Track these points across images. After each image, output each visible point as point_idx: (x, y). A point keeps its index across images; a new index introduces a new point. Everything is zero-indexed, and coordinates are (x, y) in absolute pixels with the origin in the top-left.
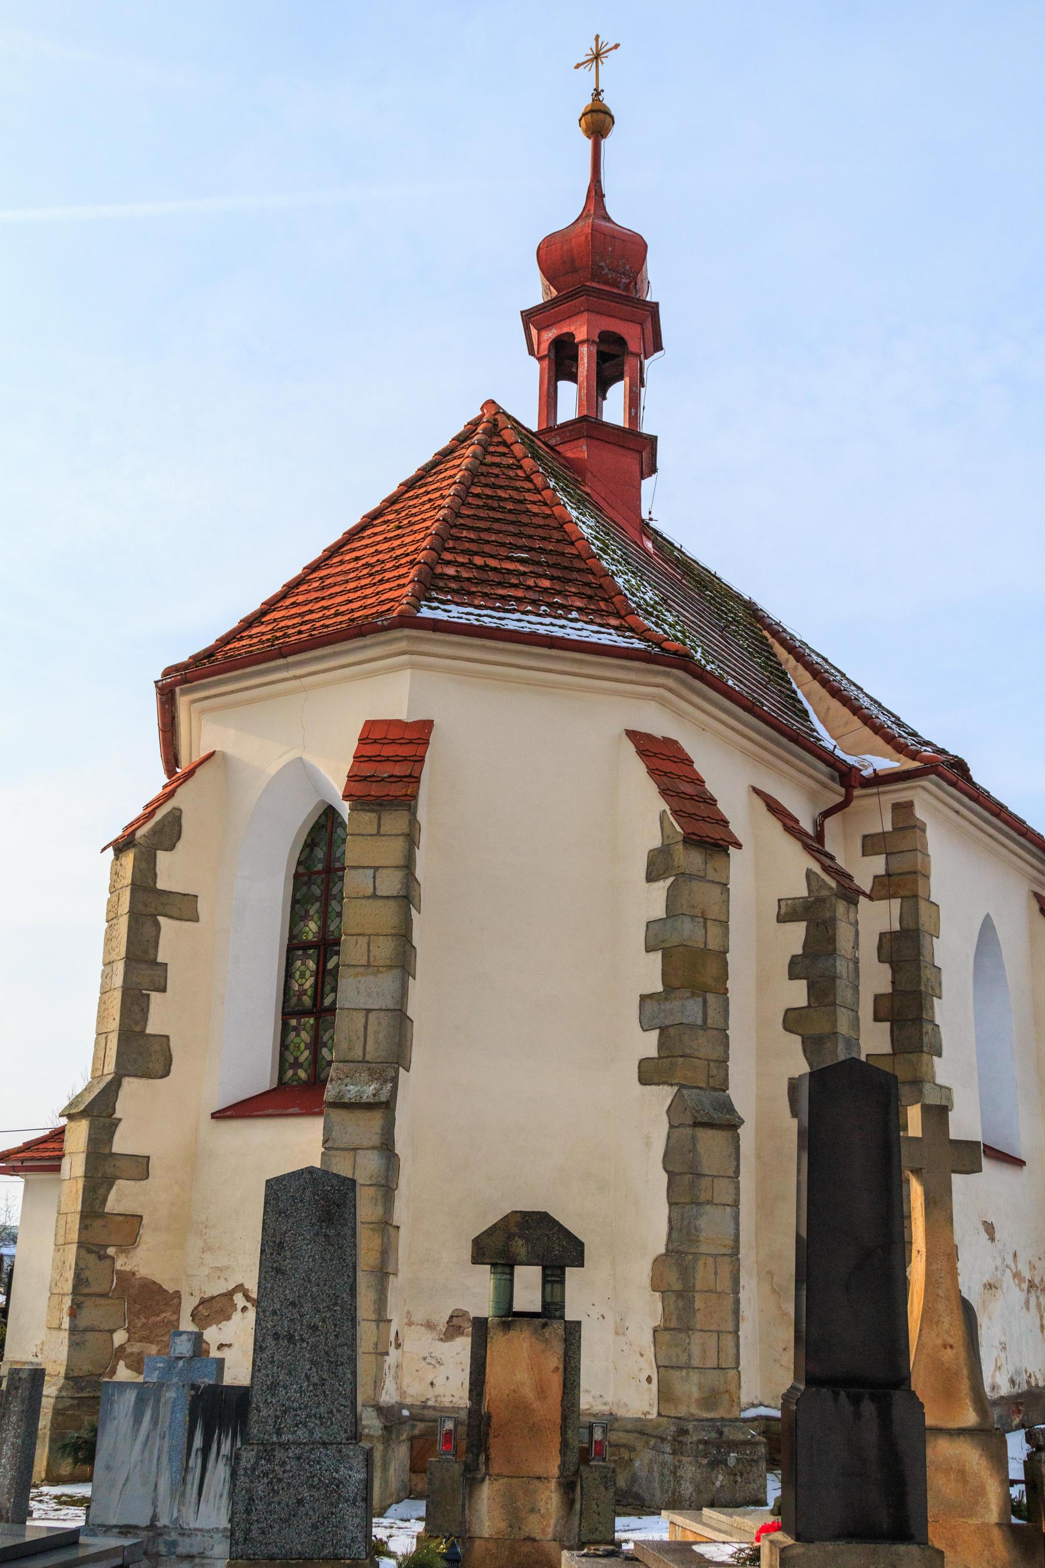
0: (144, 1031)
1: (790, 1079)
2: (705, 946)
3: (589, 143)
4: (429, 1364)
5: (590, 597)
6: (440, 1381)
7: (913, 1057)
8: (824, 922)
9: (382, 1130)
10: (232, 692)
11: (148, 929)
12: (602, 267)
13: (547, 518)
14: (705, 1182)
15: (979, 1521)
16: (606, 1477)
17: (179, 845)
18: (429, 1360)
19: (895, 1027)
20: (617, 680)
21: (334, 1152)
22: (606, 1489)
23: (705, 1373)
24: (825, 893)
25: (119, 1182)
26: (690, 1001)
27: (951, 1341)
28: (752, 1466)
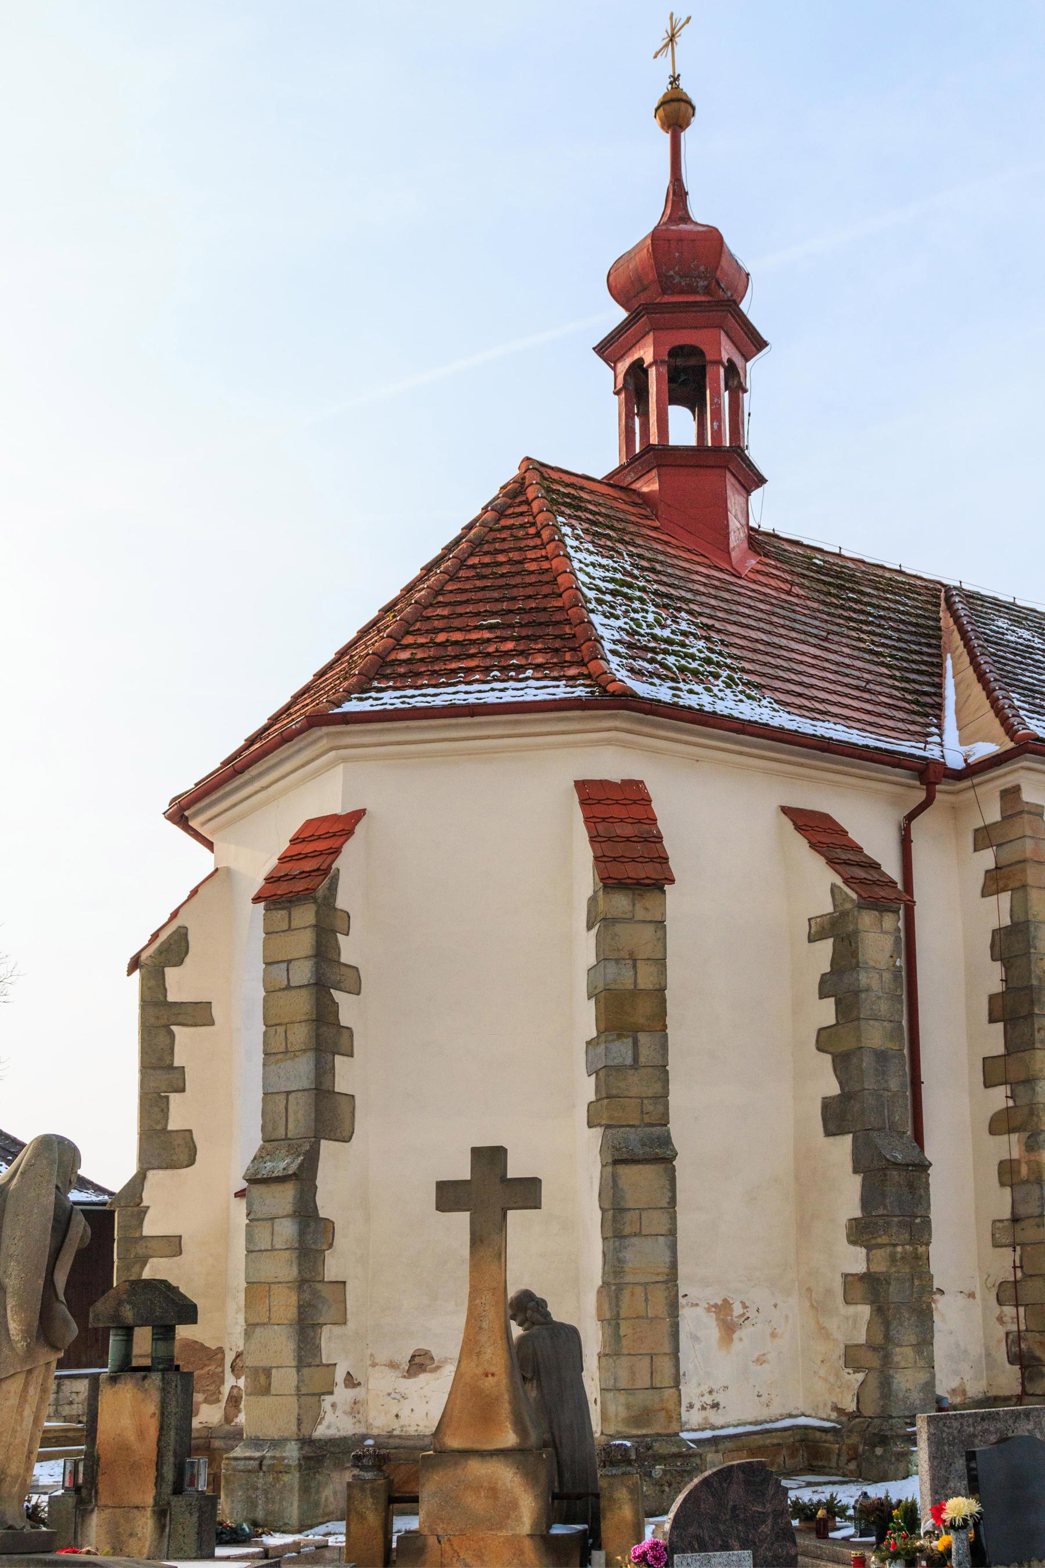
0: (166, 1128)
1: (823, 1098)
2: (635, 986)
3: (667, 138)
4: (394, 1399)
5: (556, 651)
6: (405, 1413)
7: (1026, 1055)
8: (849, 936)
9: (294, 1199)
10: (226, 810)
11: (162, 1039)
12: (671, 276)
13: (543, 573)
14: (628, 1216)
15: (510, 1533)
16: (191, 1504)
17: (187, 960)
18: (393, 1395)
19: (1008, 1027)
20: (563, 733)
21: (256, 1223)
22: (191, 1514)
23: (634, 1394)
24: (848, 906)
25: (151, 1260)
26: (617, 1043)
27: (493, 1369)
28: (682, 1477)
